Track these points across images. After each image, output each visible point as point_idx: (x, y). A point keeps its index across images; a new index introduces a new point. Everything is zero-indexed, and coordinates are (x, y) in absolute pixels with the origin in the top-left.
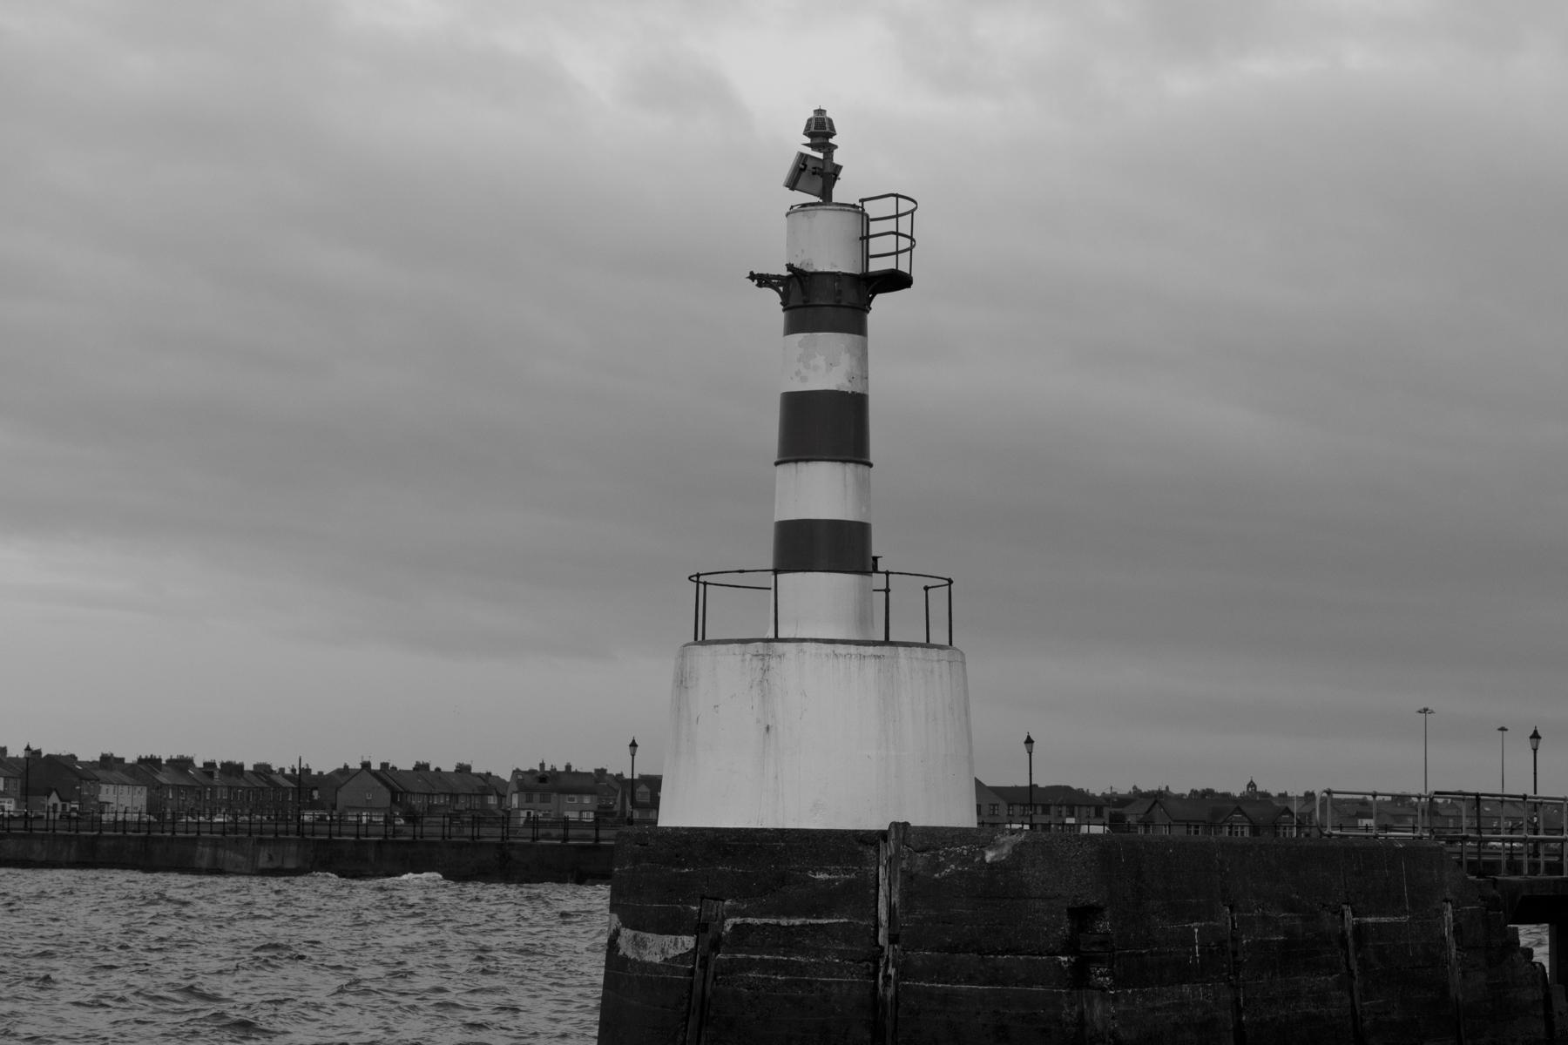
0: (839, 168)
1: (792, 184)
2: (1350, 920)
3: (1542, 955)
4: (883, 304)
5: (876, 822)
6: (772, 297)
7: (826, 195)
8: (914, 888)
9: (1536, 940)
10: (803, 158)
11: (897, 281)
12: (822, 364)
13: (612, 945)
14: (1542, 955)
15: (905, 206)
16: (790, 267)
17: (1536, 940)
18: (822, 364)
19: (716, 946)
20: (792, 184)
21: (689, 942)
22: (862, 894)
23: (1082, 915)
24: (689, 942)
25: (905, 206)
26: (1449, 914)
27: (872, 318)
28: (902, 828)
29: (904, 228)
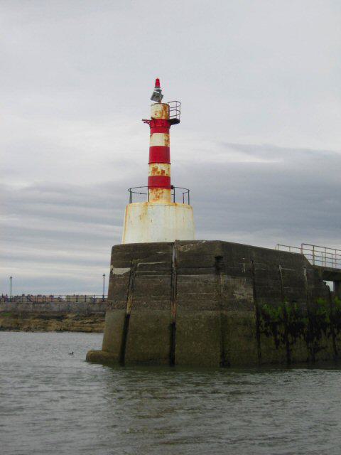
0: (123, 255)
1: (152, 99)
2: (280, 268)
3: (332, 289)
4: (173, 128)
5: (172, 240)
6: (147, 126)
7: (160, 102)
8: (181, 254)
9: (330, 284)
10: (154, 93)
11: (176, 121)
12: (159, 140)
13: (111, 272)
14: (332, 289)
15: (178, 104)
16: (152, 118)
17: (330, 284)
18: (159, 140)
19: (136, 269)
20: (152, 99)
21: (127, 270)
22: (168, 256)
23: (218, 258)
24: (127, 270)
25: (178, 104)
26: (305, 271)
27: (170, 130)
28: (178, 242)
29: (178, 108)
